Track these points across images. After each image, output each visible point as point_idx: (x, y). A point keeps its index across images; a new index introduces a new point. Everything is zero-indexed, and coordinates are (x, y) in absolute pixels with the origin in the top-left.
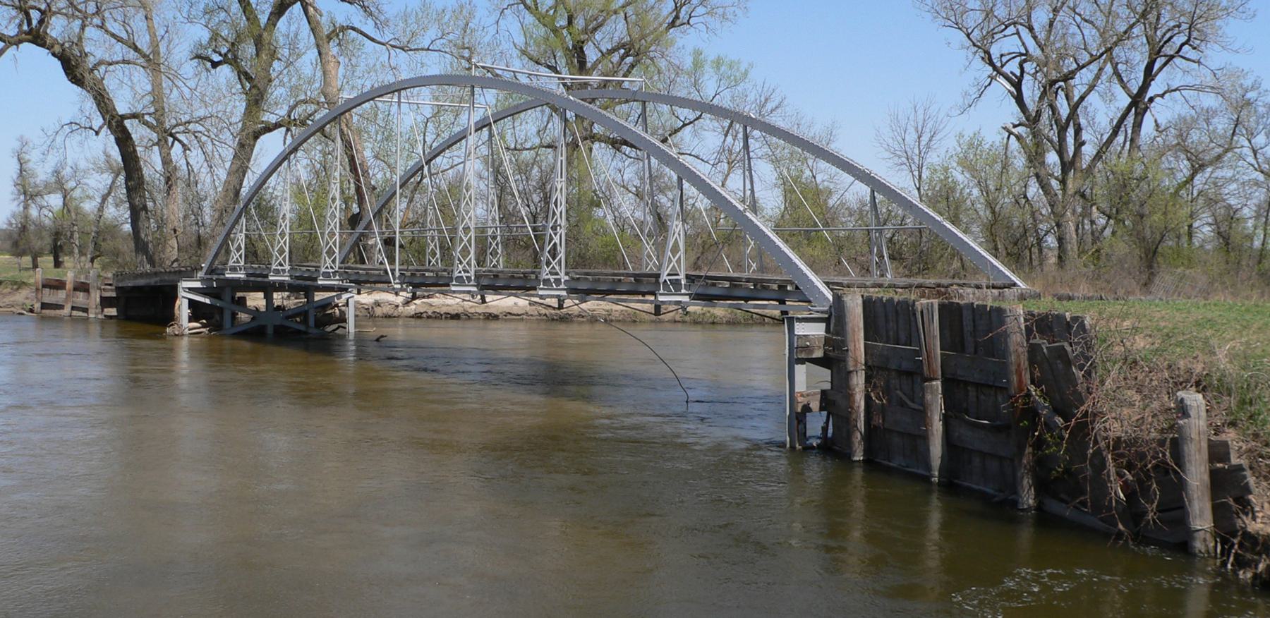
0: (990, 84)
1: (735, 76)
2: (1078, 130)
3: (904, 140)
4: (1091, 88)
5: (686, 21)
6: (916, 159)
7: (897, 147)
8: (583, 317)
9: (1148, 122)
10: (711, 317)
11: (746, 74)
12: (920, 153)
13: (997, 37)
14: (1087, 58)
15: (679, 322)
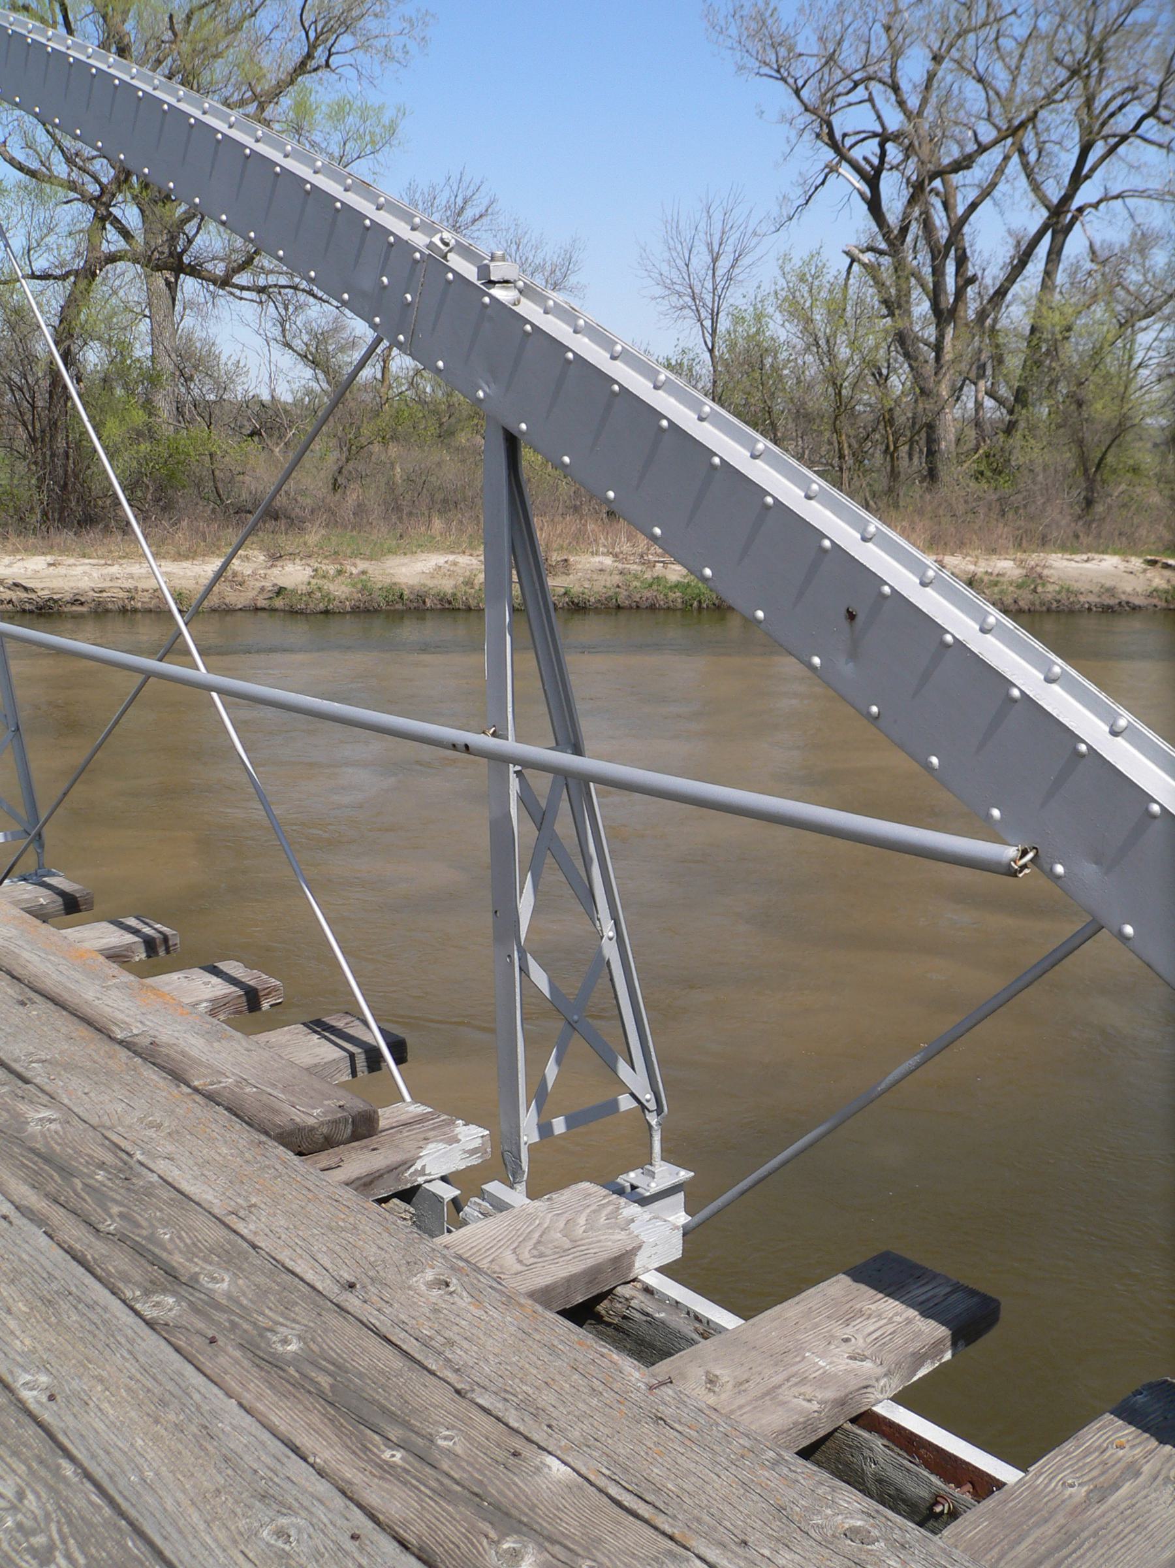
0: (823, 183)
1: (372, 134)
2: (962, 260)
3: (687, 266)
4: (987, 192)
5: (323, 61)
6: (708, 298)
7: (675, 275)
8: (82, 604)
9: (1075, 245)
10: (323, 597)
11: (392, 129)
12: (715, 289)
13: (841, 101)
14: (993, 134)
15: (263, 609)
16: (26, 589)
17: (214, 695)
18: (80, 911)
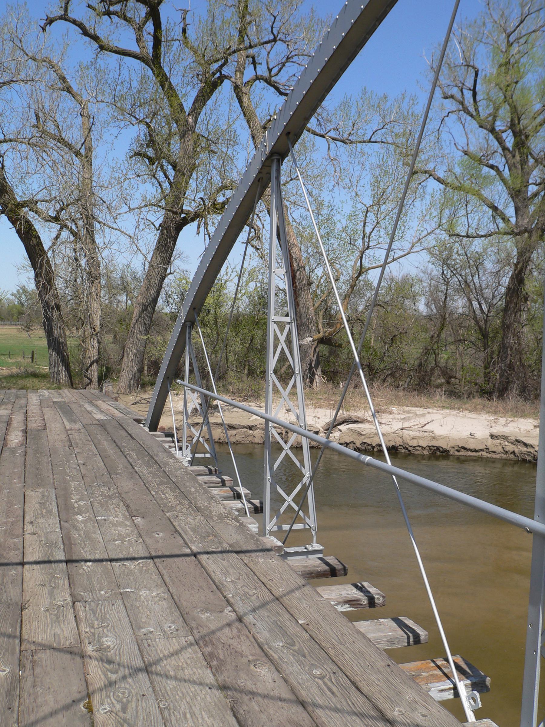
16: (526, 445)
17: (394, 477)
18: (336, 576)
